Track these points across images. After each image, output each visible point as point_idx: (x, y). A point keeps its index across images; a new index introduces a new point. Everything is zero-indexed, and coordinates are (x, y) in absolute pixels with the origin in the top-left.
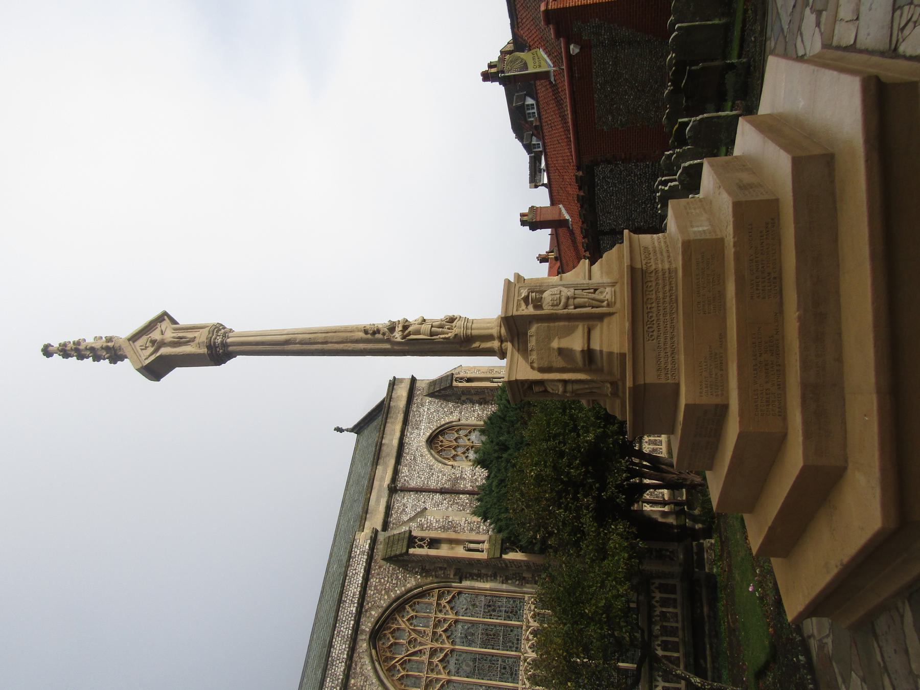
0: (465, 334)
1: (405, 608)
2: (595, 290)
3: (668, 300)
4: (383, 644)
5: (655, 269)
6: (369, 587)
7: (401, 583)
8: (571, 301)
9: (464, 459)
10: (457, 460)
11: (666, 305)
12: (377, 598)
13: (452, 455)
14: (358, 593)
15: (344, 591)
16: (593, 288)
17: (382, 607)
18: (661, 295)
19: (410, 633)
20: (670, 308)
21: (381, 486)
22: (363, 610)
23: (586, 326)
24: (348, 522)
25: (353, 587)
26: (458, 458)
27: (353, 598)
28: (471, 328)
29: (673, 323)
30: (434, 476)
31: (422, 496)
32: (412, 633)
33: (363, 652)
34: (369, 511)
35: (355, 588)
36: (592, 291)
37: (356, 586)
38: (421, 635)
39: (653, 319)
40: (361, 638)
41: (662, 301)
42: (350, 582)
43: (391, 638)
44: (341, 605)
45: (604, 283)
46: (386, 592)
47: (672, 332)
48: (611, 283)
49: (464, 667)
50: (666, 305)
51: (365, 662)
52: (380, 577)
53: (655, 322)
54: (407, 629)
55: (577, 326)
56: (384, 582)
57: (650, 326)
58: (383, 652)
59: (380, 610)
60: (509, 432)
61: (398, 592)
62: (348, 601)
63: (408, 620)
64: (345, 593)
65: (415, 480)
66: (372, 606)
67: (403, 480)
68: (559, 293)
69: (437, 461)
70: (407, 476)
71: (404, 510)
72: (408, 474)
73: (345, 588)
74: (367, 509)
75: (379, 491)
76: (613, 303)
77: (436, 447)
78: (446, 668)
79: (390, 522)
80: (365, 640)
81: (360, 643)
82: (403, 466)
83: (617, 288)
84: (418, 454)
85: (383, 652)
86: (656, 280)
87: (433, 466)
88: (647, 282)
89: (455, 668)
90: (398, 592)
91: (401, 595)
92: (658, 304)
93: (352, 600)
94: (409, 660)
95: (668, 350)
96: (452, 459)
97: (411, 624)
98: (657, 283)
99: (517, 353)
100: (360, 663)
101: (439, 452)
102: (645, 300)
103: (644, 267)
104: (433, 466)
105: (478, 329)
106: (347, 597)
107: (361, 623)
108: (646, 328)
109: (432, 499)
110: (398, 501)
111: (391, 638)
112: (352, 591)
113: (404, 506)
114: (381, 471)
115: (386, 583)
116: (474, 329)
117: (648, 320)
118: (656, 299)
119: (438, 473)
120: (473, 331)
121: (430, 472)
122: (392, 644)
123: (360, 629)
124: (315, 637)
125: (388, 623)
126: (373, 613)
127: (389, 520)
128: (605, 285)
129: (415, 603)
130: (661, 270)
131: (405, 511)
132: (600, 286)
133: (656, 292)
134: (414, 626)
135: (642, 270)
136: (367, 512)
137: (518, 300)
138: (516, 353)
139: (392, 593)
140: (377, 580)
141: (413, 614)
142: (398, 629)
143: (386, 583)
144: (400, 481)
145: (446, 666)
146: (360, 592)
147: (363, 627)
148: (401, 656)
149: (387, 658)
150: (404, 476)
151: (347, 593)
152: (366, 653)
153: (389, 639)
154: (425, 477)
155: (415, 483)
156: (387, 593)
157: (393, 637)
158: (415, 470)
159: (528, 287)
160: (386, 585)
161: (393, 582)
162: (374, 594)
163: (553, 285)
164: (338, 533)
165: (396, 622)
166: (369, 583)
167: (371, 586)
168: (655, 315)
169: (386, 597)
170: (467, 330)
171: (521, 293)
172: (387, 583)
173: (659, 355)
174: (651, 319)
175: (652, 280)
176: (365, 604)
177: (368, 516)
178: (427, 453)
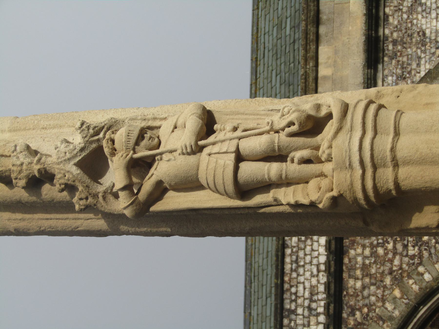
0: (373, 199)
6: (349, 270)
7: (430, 254)
12: (373, 299)
14: (322, 288)
15: (286, 286)
17: (391, 318)
24: (280, 26)
25: (308, 274)
27: (311, 301)
28: (394, 158)
34: (324, 17)
35: (312, 276)
37: (315, 272)
42: (297, 262)
44: (286, 321)
46: (394, 279)
52: (371, 244)
56: (386, 254)
61: (427, 277)
62: (300, 311)
64: (289, 290)
73: (286, 279)
74: (318, 12)
79: (386, 38)
90: (427, 277)
93: (310, 308)
106: (295, 301)
112: (307, 285)
115: (390, 256)
116: (408, 162)
120: (403, 172)
124: (254, 313)
127: (381, 33)
136: (317, 22)
139: (411, 282)
140: (367, 252)
143: (390, 256)
146: (327, 285)
151: (293, 290)
160: (391, 261)
161: (411, 252)
162: (364, 287)
164: (260, 53)
166: (346, 260)
169: (397, 293)
170: (380, 171)
172: (394, 257)
176: (345, 315)
177: (322, 30)
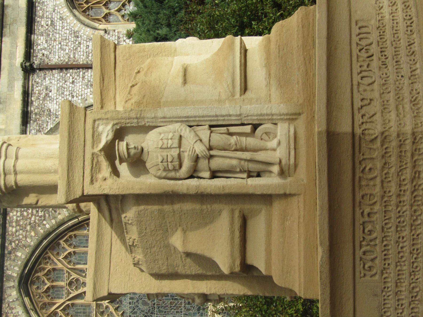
1: (59, 244)
2: (255, 127)
3: (407, 197)
4: (38, 288)
5: (383, 133)
6: (10, 223)
7: (49, 215)
8: (203, 164)
9: (120, 18)
10: (111, 20)
11: (404, 209)
12: (21, 236)
13: (103, 15)
16: (250, 122)
17: (29, 246)
18: (393, 188)
19: (69, 273)
20: (412, 216)
21: (11, 65)
22: (6, 252)
23: (237, 214)
26: (111, 18)
29: (417, 244)
30: (82, 46)
31: (69, 75)
32: (72, 273)
33: (13, 301)
36: (248, 129)
38: (84, 274)
39: (374, 235)
40: (9, 285)
41: (394, 200)
43: (46, 281)
45: (273, 115)
46: (32, 227)
47: (413, 263)
48: (287, 114)
49: (141, 306)
50: (404, 209)
51: (18, 312)
53: (377, 241)
54: (65, 269)
55: (220, 212)
56: (28, 215)
57: (368, 248)
58: (39, 298)
59: (28, 251)
60: (169, 25)
63: (66, 258)
65: (57, 54)
66: (17, 245)
67: (41, 55)
68: (176, 145)
69: (84, 24)
70: (45, 49)
71: (47, 95)
72: (46, 46)
75: (10, 73)
76: (292, 167)
77: (79, 4)
78: (119, 309)
79: (32, 112)
80: (13, 287)
81: (8, 292)
82: (37, 35)
83: (301, 122)
84: (56, 17)
85: (39, 298)
86: (383, 157)
87: (78, 32)
88: (364, 159)
89: (130, 308)
90: (48, 226)
91: (51, 230)
92: (385, 206)
94: (73, 305)
95: (404, 295)
96: (103, 20)
97: (69, 262)
98: (385, 164)
99: (109, 228)
100: (12, 314)
101: (84, 11)
102: (358, 198)
103: (358, 131)
104: (78, 32)
105: (29, 172)
107: (5, 268)
108: (359, 253)
109: (83, 77)
110: (37, 83)
111: (46, 281)
113: (47, 90)
114: (9, 45)
115: (30, 216)
116: (22, 172)
117: (364, 238)
118: (383, 197)
119: (87, 42)
120: (19, 177)
121: (76, 40)
122: (48, 288)
123: (5, 274)
125: (40, 264)
126: (19, 254)
128: (275, 117)
129: (71, 237)
130: (395, 135)
131: (49, 97)
132: (265, 120)
133: (382, 182)
134: (74, 264)
135: (353, 135)
137: (93, 154)
138: (107, 229)
139: (40, 228)
140: (19, 214)
141: (70, 250)
142: (54, 269)
143: (30, 216)
144: (37, 56)
145: (118, 307)
147: (9, 272)
148: (62, 301)
149: (45, 304)
150: (41, 50)
152: (17, 302)
153: (43, 282)
154: (69, 49)
155: (57, 57)
156: (33, 228)
157: (48, 279)
158: (55, 40)
159: (113, 120)
160: (30, 218)
161: (40, 214)
162: (16, 231)
163: (164, 118)
165: (50, 262)
166: (8, 218)
167: (11, 222)
168: (378, 227)
169: (33, 234)
170: (8, 176)
171: (100, 135)
173: (384, 304)
174: (370, 234)
175: (374, 156)
176: (7, 245)
178: (68, 15)
